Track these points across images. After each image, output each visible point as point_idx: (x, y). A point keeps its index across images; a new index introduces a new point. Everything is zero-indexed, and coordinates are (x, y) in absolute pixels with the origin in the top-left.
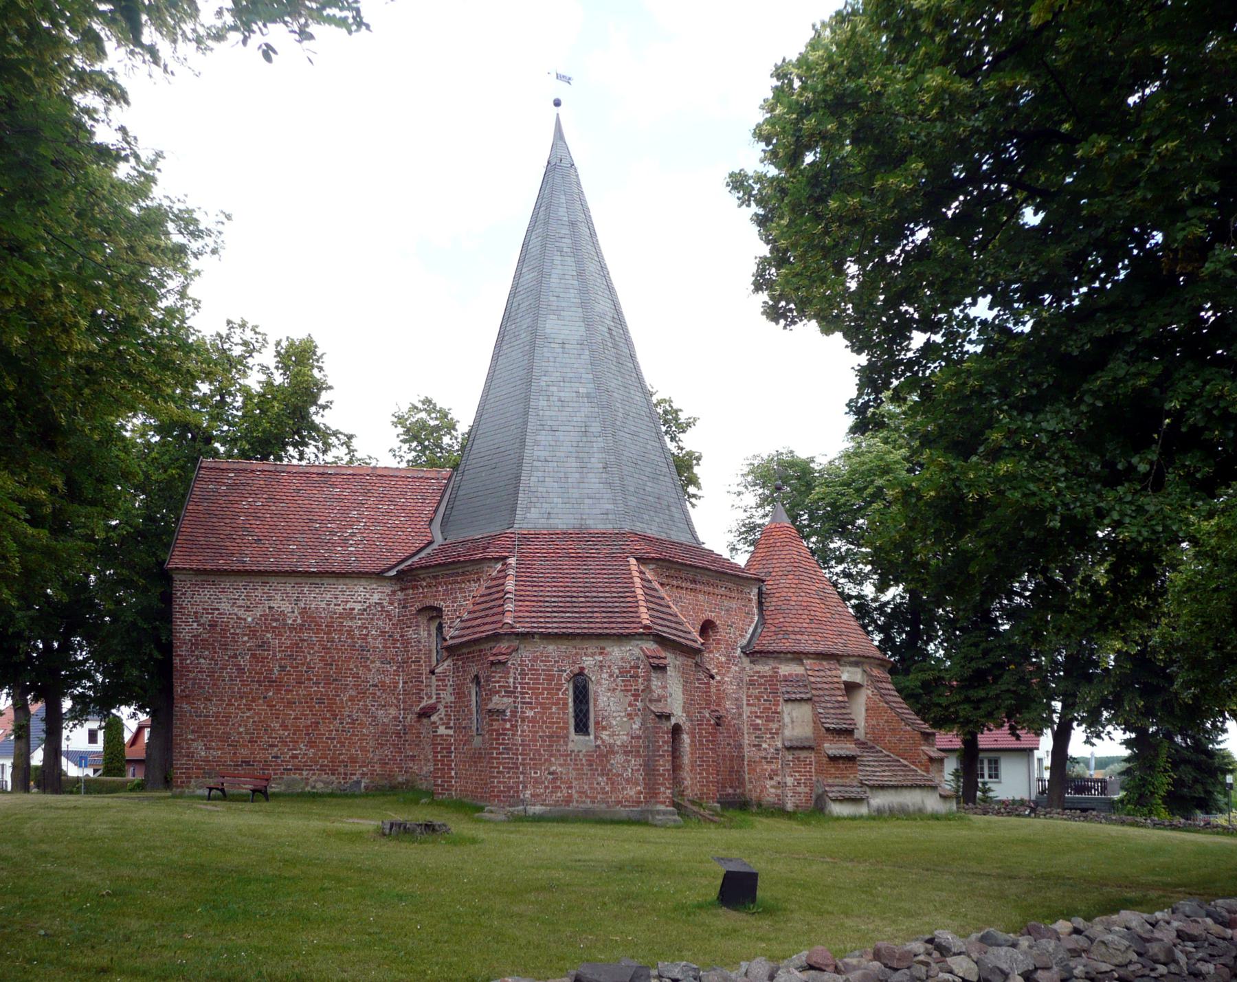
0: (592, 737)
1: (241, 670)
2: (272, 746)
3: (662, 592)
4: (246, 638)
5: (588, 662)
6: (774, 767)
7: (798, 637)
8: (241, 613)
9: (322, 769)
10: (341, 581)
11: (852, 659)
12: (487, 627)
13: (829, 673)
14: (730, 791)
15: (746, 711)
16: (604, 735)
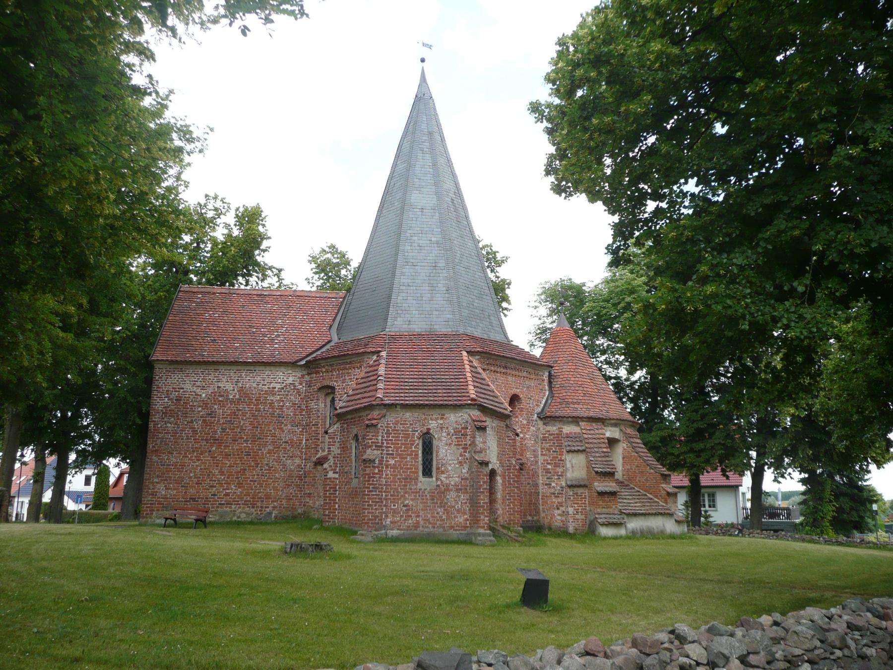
0: (434, 479)
1: (195, 432)
3: (484, 375)
5: (433, 424)
7: (576, 406)
8: (198, 391)
10: (268, 368)
13: (597, 431)
14: (530, 518)
15: (541, 459)
16: (443, 477)
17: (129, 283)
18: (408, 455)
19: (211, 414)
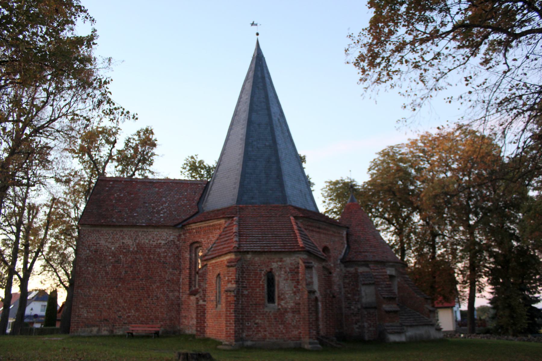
0: (276, 304)
1: (107, 273)
2: (119, 311)
3: (306, 232)
4: (110, 258)
5: (274, 265)
6: (357, 318)
7: (366, 254)
8: (109, 246)
9: (142, 323)
10: (156, 230)
11: (391, 264)
12: (225, 249)
13: (381, 271)
16: (282, 303)
18: (257, 287)
19: (118, 261)
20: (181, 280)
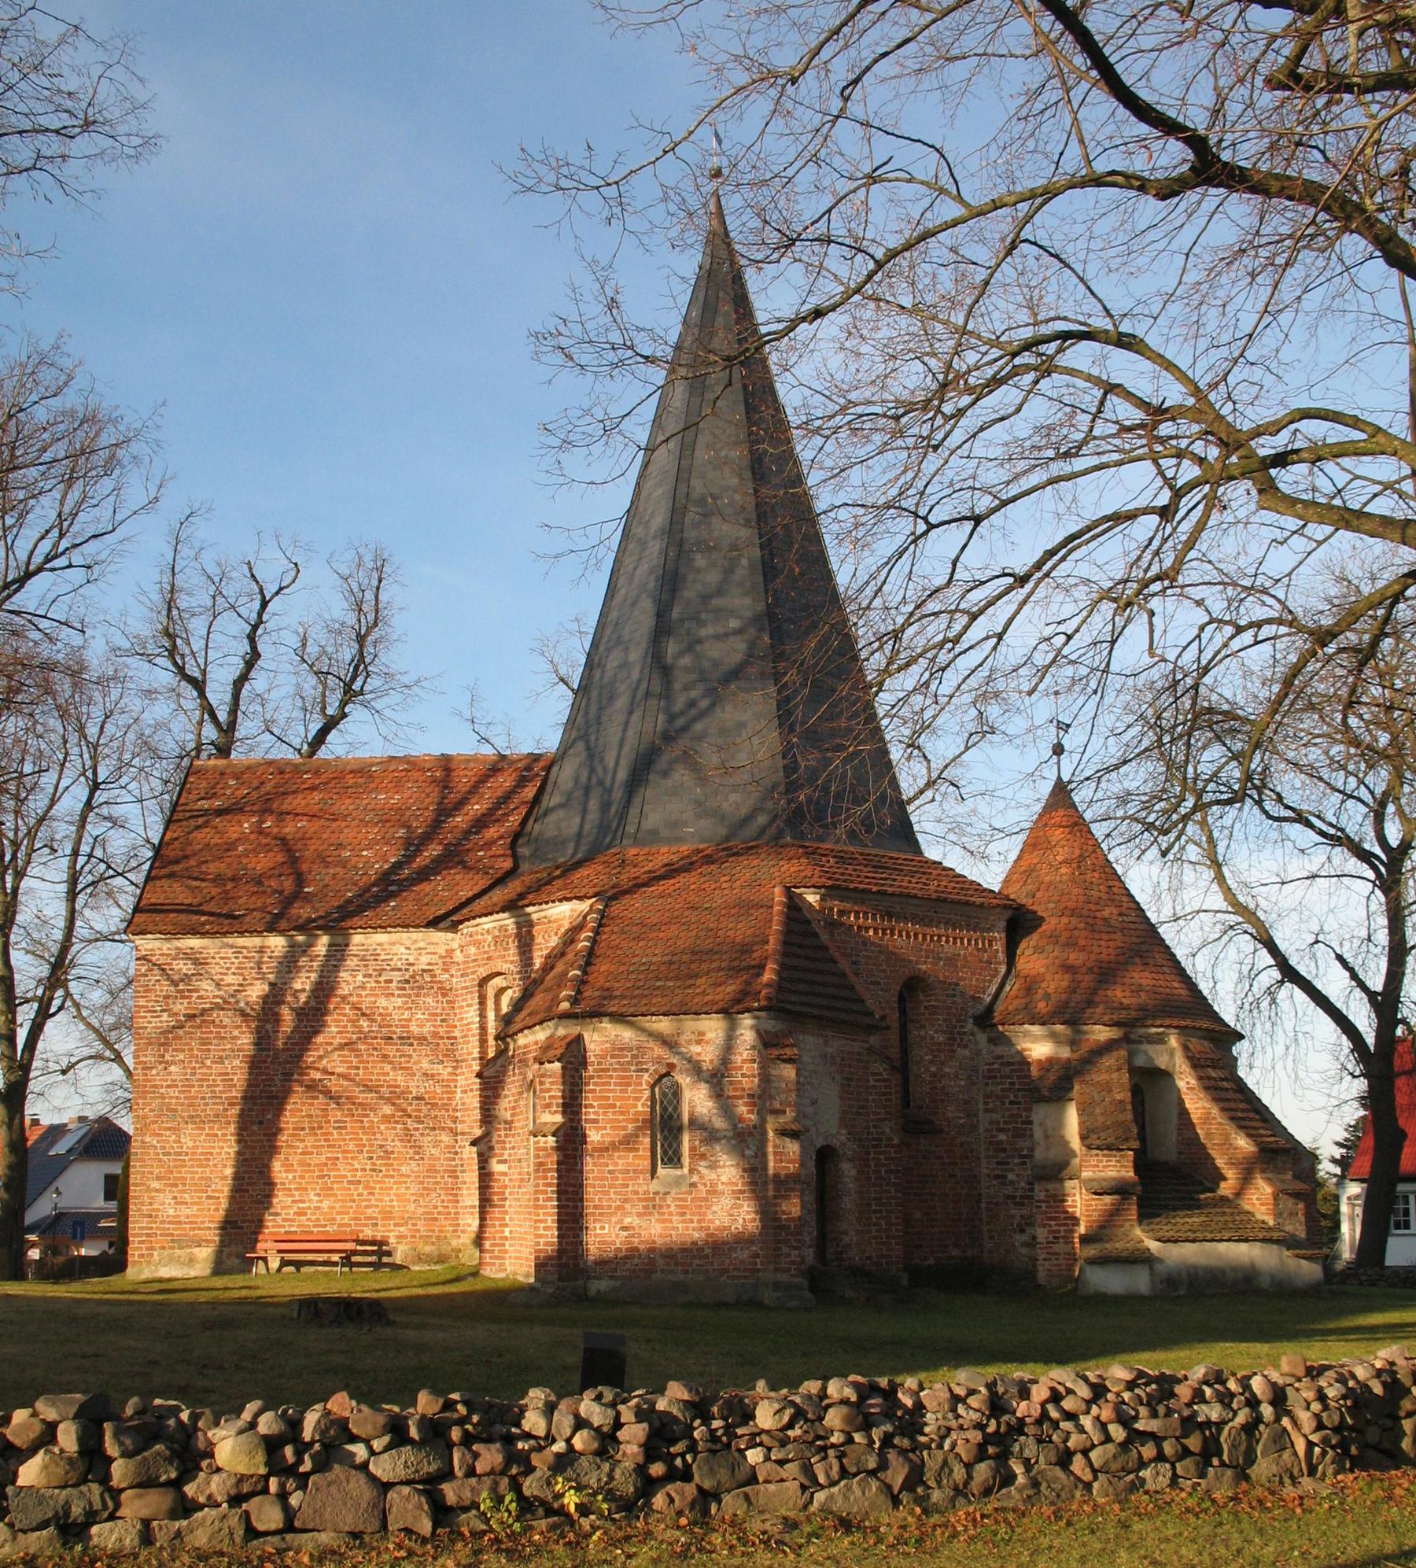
14: (955, 1252)
15: (984, 1120)
17: (717, 432)
20: (458, 1095)
